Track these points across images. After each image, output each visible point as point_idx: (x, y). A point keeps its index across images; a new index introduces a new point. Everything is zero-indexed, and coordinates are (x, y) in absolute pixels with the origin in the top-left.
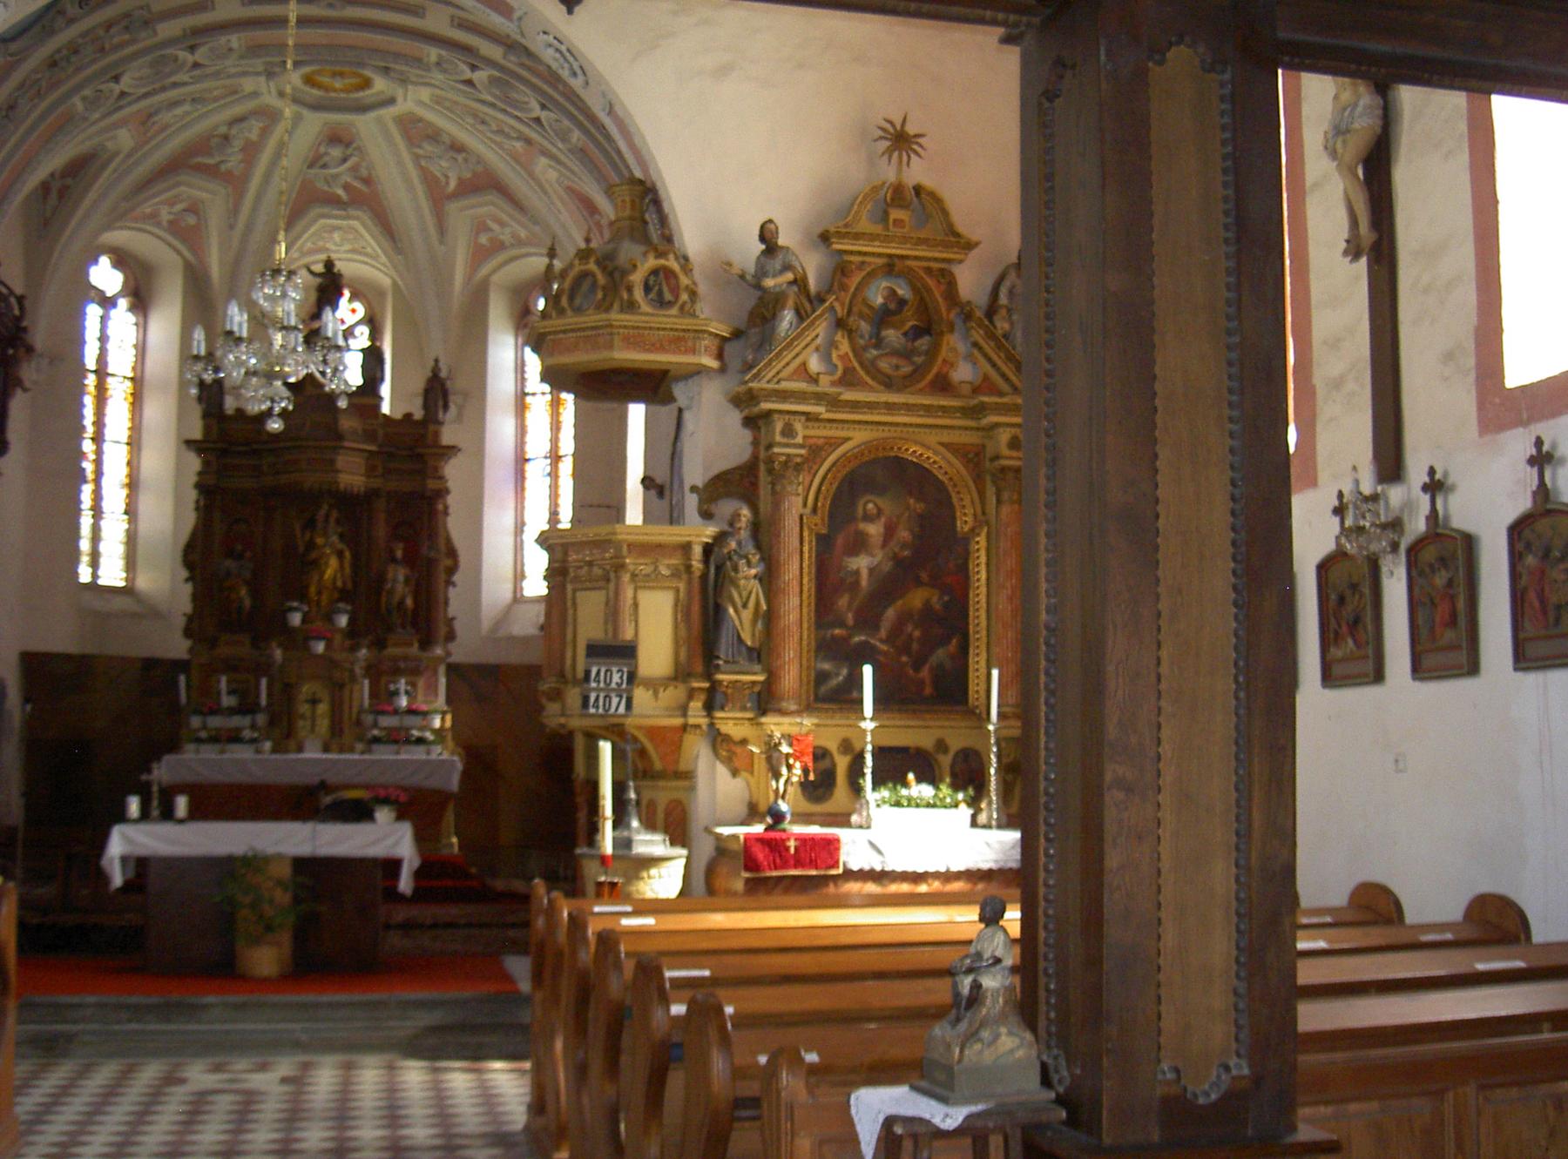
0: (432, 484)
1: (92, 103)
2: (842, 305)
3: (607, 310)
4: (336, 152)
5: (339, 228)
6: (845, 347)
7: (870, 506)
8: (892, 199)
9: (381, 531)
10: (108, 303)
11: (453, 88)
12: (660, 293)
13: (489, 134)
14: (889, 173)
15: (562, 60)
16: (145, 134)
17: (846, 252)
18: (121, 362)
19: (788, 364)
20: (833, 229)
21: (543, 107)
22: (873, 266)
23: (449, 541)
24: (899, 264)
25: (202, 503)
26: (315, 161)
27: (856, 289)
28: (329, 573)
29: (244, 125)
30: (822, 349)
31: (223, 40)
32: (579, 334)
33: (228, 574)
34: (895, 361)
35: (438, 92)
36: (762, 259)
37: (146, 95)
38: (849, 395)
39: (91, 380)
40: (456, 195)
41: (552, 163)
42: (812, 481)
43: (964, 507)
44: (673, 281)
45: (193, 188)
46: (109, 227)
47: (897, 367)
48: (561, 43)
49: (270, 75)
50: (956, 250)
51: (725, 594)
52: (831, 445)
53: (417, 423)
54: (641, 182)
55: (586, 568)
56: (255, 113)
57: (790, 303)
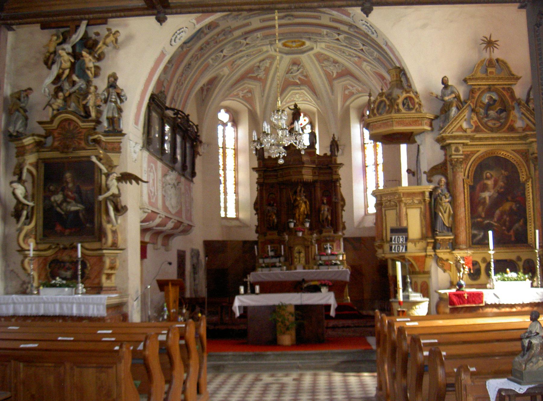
0: (335, 177)
1: (214, 60)
2: (473, 104)
3: (391, 113)
4: (295, 68)
5: (298, 93)
7: (488, 174)
9: (319, 193)
10: (225, 125)
11: (332, 42)
12: (408, 105)
14: (486, 55)
15: (368, 29)
18: (230, 144)
20: (468, 78)
21: (363, 45)
25: (259, 189)
26: (288, 72)
27: (478, 97)
28: (302, 209)
34: (493, 122)
36: (443, 90)
37: (232, 56)
46: (223, 100)
53: (328, 157)
54: (399, 68)
55: (389, 203)
56: (267, 58)
57: (454, 105)
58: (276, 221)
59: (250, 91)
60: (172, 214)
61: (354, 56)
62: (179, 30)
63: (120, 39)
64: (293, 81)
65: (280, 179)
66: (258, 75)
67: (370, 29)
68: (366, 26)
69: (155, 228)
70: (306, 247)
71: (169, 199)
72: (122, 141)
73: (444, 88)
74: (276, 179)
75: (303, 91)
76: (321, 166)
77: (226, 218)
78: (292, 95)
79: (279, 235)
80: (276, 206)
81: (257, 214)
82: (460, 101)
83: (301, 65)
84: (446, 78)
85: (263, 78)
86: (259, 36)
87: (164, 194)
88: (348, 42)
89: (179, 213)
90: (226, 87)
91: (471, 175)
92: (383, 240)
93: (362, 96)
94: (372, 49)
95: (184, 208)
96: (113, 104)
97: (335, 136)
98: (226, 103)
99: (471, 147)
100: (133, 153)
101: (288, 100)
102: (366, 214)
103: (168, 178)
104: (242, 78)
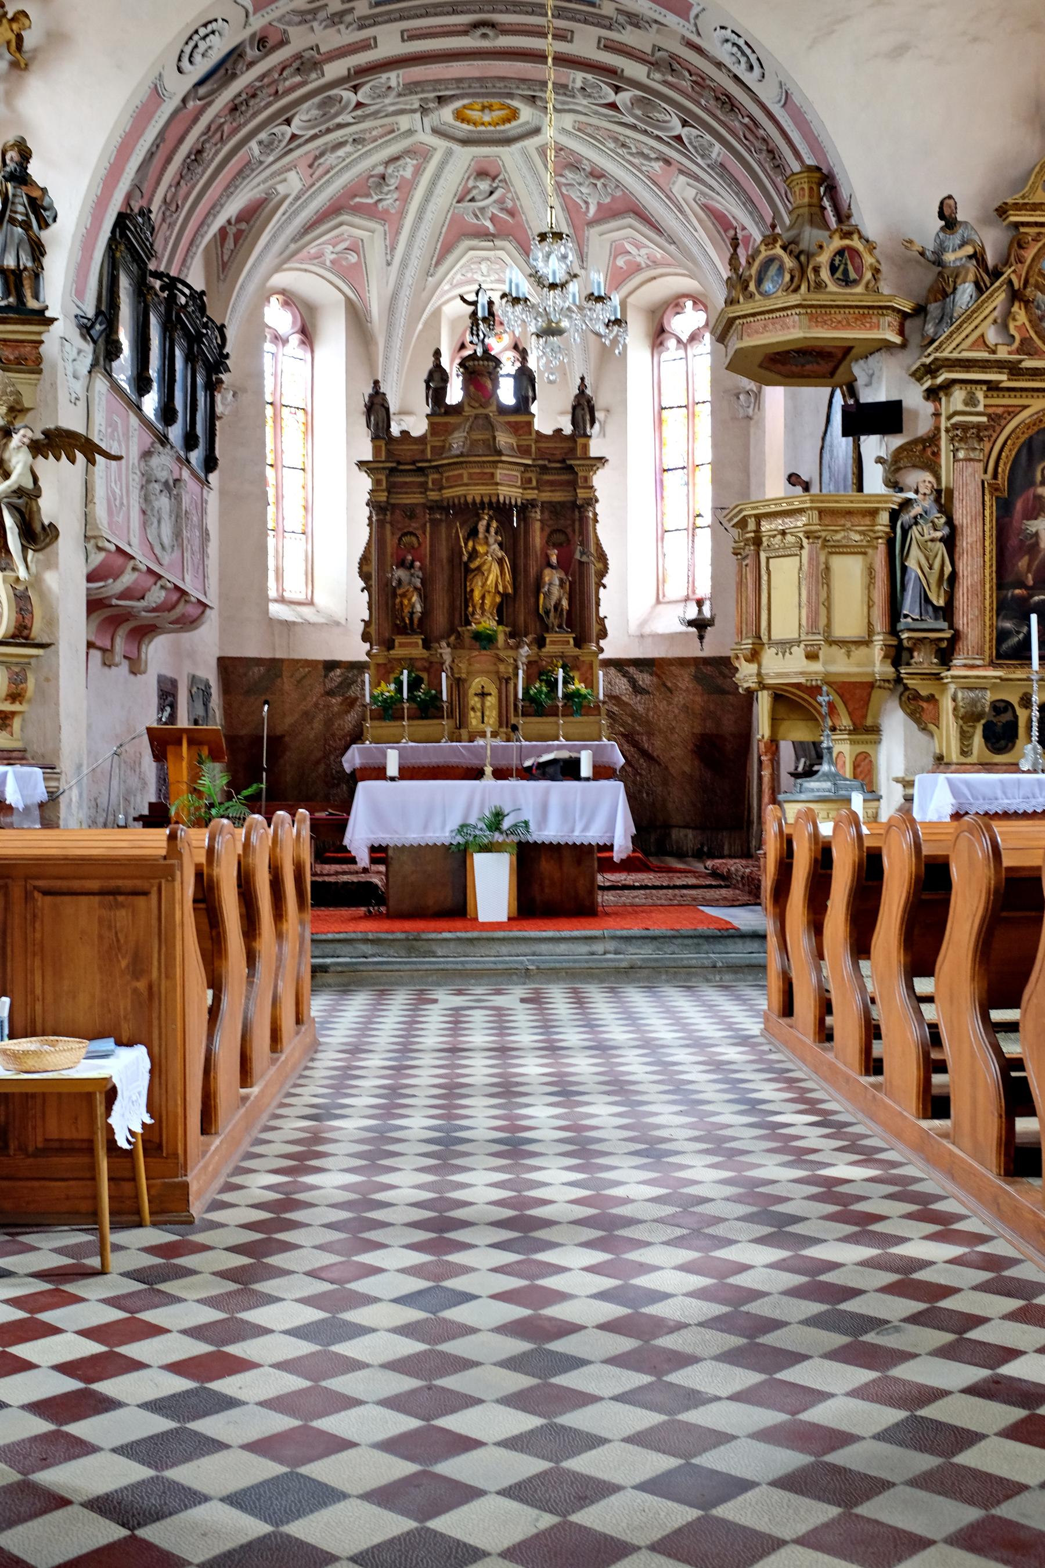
1: (267, 147)
2: (1019, 277)
4: (484, 186)
5: (488, 259)
9: (537, 539)
11: (596, 113)
12: (846, 272)
16: (311, 176)
19: (967, 336)
20: (1010, 201)
21: (685, 124)
23: (598, 545)
25: (374, 519)
27: (1033, 260)
28: (492, 578)
29: (401, 162)
30: (999, 321)
31: (384, 76)
32: (767, 316)
33: (400, 582)
36: (941, 235)
38: (1029, 363)
40: (591, 224)
41: (691, 181)
42: (992, 449)
44: (857, 260)
46: (278, 269)
48: (739, 36)
49: (424, 111)
52: (1009, 413)
54: (818, 169)
55: (779, 537)
56: (408, 152)
57: (971, 277)
58: (418, 608)
61: (653, 156)
62: (205, 25)
63: (31, 39)
64: (475, 224)
65: (433, 495)
66: (380, 200)
67: (744, 54)
68: (734, 44)
69: (114, 602)
70: (500, 679)
72: (44, 337)
73: (942, 229)
74: (421, 493)
75: (501, 254)
76: (546, 462)
78: (471, 261)
79: (427, 645)
81: (367, 588)
82: (986, 270)
83: (501, 177)
84: (951, 202)
85: (393, 211)
86: (393, 83)
87: (144, 506)
91: (1004, 471)
93: (662, 275)
94: (708, 137)
96: (20, 230)
97: (586, 382)
98: (280, 280)
99: (1007, 394)
100: (71, 379)
101: (459, 277)
104: (334, 210)
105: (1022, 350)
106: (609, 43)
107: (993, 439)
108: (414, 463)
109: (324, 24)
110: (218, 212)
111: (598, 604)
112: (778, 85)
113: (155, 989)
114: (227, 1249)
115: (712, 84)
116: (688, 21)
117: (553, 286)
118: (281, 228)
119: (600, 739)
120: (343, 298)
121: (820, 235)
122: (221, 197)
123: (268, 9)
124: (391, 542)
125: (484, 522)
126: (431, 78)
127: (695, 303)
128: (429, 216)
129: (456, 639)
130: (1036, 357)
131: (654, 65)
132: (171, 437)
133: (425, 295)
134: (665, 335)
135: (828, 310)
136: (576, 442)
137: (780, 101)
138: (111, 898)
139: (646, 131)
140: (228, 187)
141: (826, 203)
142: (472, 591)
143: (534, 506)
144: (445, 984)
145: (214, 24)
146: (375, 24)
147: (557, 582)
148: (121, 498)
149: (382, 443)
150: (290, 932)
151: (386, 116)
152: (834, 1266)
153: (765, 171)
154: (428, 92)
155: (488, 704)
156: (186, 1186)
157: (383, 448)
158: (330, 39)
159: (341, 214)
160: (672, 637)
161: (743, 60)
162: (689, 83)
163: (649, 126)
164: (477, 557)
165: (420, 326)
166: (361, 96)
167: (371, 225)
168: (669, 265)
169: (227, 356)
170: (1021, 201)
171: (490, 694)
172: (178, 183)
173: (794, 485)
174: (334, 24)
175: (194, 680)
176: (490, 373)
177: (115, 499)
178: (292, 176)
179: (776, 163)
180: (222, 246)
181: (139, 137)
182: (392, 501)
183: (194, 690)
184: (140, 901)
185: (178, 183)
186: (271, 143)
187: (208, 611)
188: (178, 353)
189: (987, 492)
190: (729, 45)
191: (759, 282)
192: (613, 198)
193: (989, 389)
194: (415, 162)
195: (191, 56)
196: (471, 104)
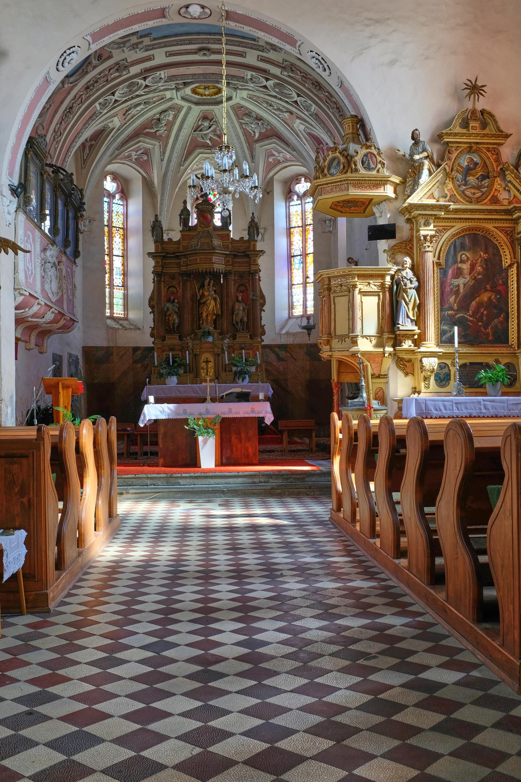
0: (253, 268)
1: (103, 105)
3: (346, 173)
4: (206, 124)
5: (208, 158)
6: (450, 186)
7: (463, 256)
8: (471, 117)
9: (233, 289)
10: (111, 196)
11: (258, 90)
13: (273, 111)
14: (469, 105)
15: (319, 64)
16: (125, 119)
17: (450, 142)
18: (117, 222)
20: (444, 132)
21: (299, 95)
22: (462, 148)
23: (261, 291)
24: (474, 147)
26: (197, 129)
27: (455, 159)
31: (158, 73)
32: (332, 185)
34: (473, 191)
35: (251, 93)
37: (126, 101)
39: (106, 229)
40: (257, 141)
43: (506, 255)
45: (146, 143)
46: (110, 163)
47: (474, 194)
48: (319, 55)
49: (177, 89)
50: (501, 138)
51: (400, 295)
53: (246, 241)
54: (356, 117)
55: (339, 287)
56: (171, 108)
59: (146, 152)
60: (52, 302)
62: (69, 49)
65: (183, 269)
67: (321, 63)
68: (317, 59)
69: (30, 319)
71: (49, 281)
73: (413, 144)
74: (178, 267)
77: (111, 317)
79: (181, 339)
80: (178, 303)
81: (153, 312)
84: (417, 132)
85: (164, 136)
86: (163, 76)
87: (43, 274)
88: (278, 90)
89: (60, 302)
90: (115, 145)
92: (330, 334)
94: (309, 102)
95: (65, 296)
98: (110, 167)
102: (290, 316)
103: (48, 253)
104: (136, 134)
105: (451, 200)
106: (263, 58)
107: (437, 242)
108: (174, 253)
109: (129, 49)
110: (81, 136)
111: (261, 319)
112: (337, 78)
113: (31, 501)
114: (63, 624)
115: (310, 77)
116: (295, 48)
117: (225, 171)
118: (111, 144)
119: (258, 382)
120: (141, 176)
121: (357, 147)
122: (82, 129)
123: (99, 42)
124: (164, 290)
125: (208, 281)
126: (180, 74)
127: (305, 179)
128: (181, 138)
129: (194, 336)
130: (457, 204)
131: (284, 68)
132: (56, 241)
133: (179, 174)
134: (292, 194)
135: (361, 182)
136: (250, 243)
137: (338, 85)
138: (10, 459)
139: (281, 99)
140: (85, 124)
141: (360, 132)
142: (202, 313)
143: (230, 274)
144: (184, 498)
145: (74, 48)
146: (153, 49)
147: (241, 309)
148: (32, 270)
149: (159, 244)
150: (105, 474)
151: (160, 91)
152: (349, 628)
153: (335, 117)
154: (179, 80)
155: (210, 366)
156: (47, 595)
157: (160, 247)
158: (132, 56)
159: (139, 137)
160: (294, 335)
161: (321, 66)
162: (300, 77)
163: (283, 95)
164: (204, 297)
165: (177, 189)
166: (147, 82)
167: (154, 142)
168: (293, 161)
169: (84, 204)
170: (449, 132)
171: (210, 362)
172: (61, 123)
173: (350, 263)
174: (134, 48)
175: (70, 355)
176: (210, 212)
177: (29, 271)
178: (116, 119)
179: (341, 114)
180: (83, 152)
181: (38, 102)
182: (164, 271)
183: (71, 360)
184: (24, 461)
185: (61, 123)
186: (105, 104)
187: (76, 323)
188: (60, 202)
189: (435, 266)
190: (314, 60)
191: (329, 169)
192: (267, 129)
193: (435, 218)
194: (174, 113)
195: (63, 63)
196: (199, 86)
